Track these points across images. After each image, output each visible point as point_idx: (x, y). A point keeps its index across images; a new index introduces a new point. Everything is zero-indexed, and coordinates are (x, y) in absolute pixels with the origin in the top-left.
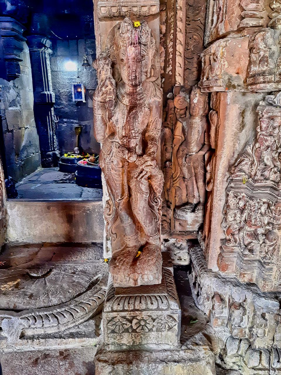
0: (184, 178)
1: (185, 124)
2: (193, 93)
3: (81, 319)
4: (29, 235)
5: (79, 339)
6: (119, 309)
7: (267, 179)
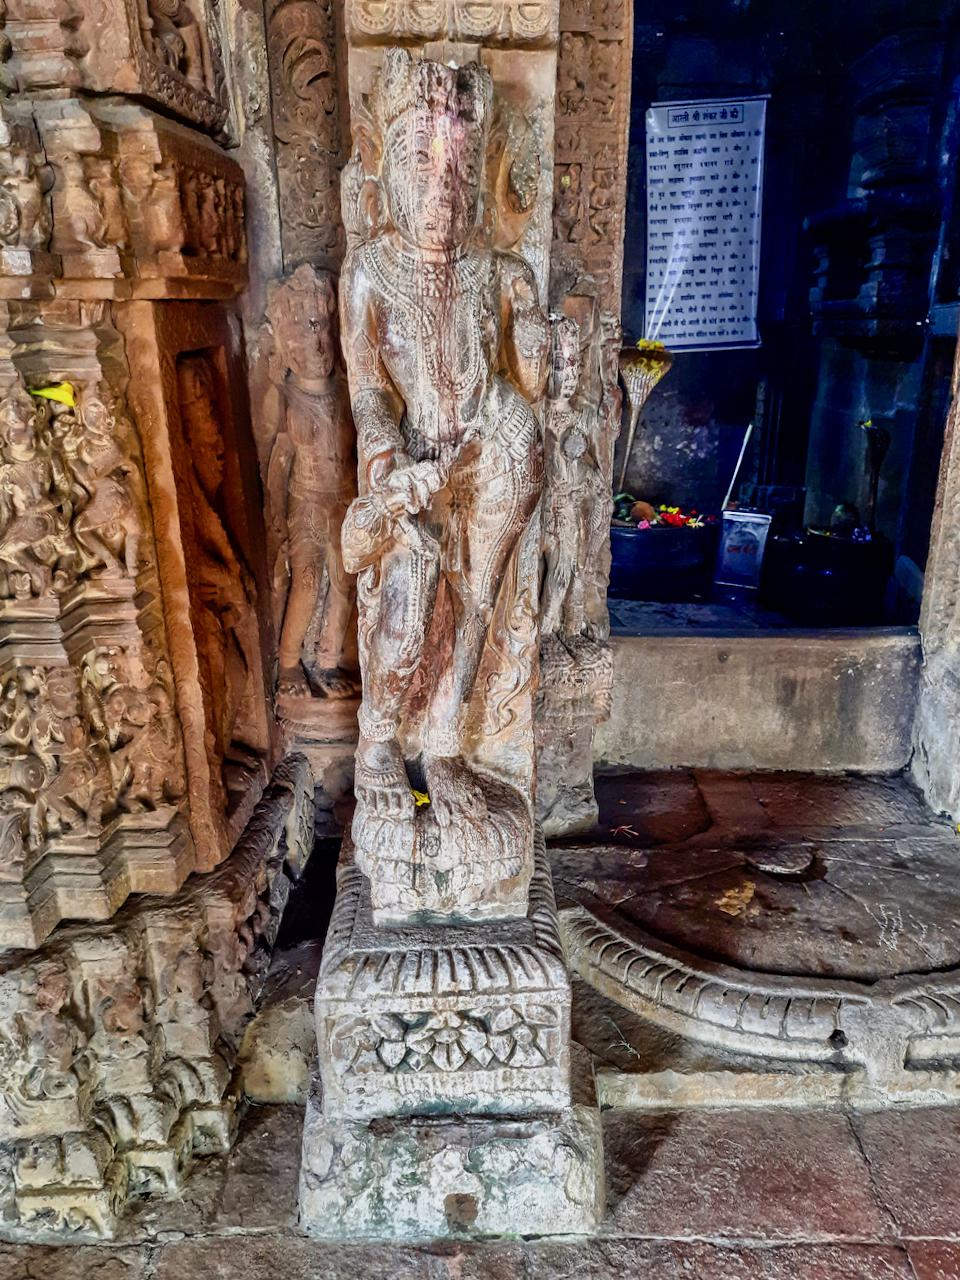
4: (645, 744)
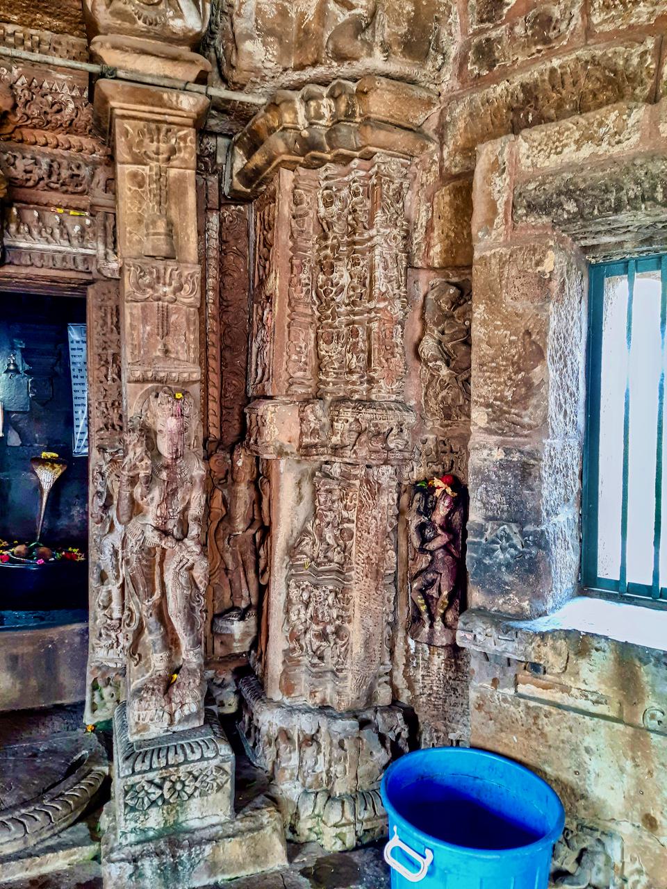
0: (226, 569)
1: (226, 492)
2: (235, 453)
3: (64, 821)
5: (66, 852)
6: (144, 768)
7: (331, 561)
